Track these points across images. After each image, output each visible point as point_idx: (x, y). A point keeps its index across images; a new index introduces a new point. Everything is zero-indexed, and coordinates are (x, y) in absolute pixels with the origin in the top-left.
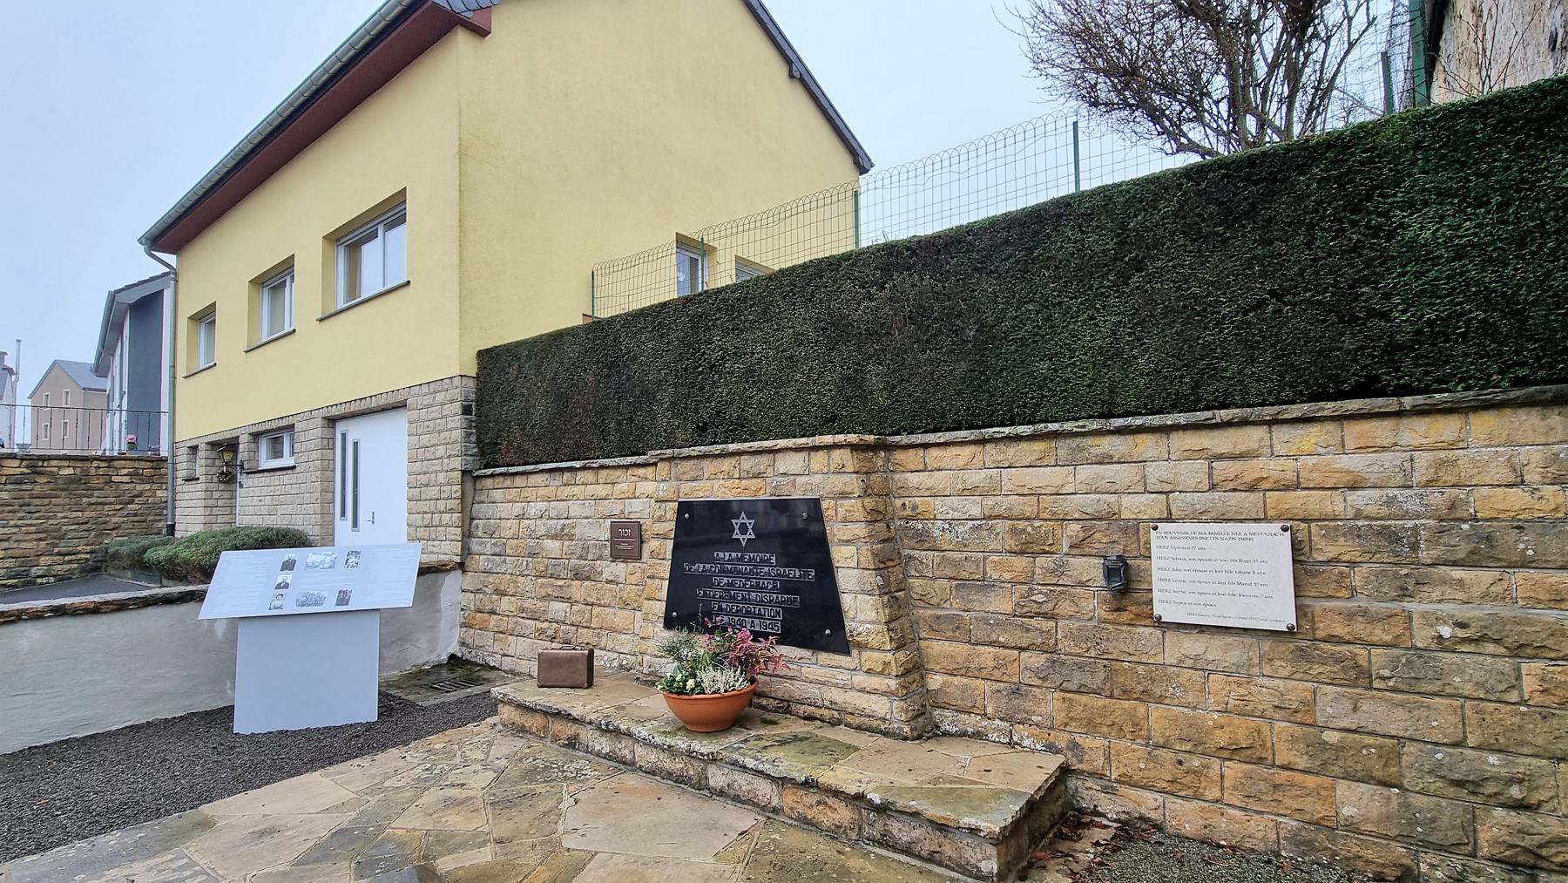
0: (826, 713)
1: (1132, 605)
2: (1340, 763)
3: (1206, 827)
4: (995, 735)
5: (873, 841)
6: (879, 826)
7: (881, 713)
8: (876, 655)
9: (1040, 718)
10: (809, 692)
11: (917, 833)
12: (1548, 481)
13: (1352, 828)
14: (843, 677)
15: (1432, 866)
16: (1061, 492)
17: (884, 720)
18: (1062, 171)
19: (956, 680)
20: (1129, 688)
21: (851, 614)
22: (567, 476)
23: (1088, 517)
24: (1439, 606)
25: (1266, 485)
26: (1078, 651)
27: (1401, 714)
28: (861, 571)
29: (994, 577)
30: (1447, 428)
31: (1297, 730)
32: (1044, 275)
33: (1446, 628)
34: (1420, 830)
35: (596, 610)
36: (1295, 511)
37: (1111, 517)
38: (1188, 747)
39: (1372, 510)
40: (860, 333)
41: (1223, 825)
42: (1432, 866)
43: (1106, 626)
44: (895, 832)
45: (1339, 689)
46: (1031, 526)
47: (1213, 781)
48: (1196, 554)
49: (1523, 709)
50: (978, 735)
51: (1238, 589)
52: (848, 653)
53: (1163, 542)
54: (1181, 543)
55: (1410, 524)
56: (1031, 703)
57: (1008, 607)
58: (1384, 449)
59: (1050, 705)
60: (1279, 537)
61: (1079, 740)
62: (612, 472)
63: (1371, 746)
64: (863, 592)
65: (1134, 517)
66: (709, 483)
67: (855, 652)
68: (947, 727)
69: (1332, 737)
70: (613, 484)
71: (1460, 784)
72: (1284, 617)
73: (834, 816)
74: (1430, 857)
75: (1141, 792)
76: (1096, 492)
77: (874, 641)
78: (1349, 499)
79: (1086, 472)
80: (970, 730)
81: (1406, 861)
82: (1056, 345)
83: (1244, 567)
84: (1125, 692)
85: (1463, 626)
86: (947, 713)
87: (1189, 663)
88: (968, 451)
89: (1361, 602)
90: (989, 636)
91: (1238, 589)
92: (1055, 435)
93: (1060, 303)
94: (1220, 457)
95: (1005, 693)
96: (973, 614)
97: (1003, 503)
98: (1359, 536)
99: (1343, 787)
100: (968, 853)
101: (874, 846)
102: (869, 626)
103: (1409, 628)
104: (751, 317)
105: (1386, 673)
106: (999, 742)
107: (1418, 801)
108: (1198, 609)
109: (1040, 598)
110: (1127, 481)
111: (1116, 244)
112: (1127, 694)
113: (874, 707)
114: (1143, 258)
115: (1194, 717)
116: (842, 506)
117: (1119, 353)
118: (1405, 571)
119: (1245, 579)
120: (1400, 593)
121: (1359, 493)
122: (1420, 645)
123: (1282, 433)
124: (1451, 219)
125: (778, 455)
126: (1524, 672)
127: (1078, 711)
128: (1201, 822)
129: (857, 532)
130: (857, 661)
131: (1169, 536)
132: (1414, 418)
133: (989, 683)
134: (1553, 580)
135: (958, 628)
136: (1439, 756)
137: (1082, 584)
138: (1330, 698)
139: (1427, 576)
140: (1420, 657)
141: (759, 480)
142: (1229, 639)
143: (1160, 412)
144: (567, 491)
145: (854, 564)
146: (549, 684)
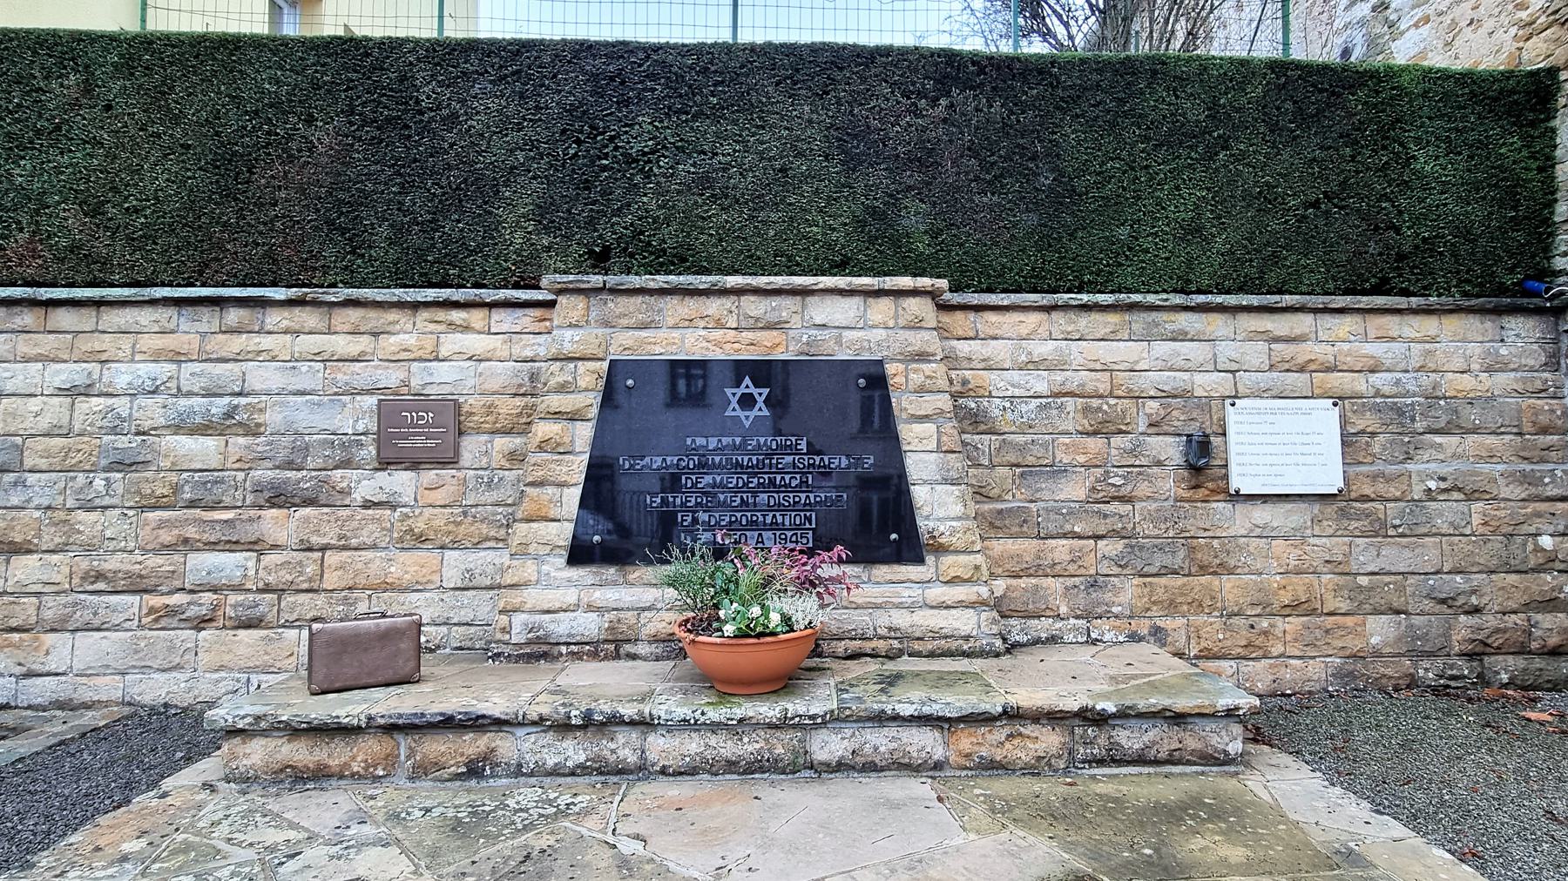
0: (881, 645)
1: (1208, 481)
2: (1371, 601)
3: (1274, 681)
4: (1071, 636)
5: (1090, 762)
6: (1102, 741)
7: (966, 629)
8: (963, 558)
9: (1120, 608)
10: (854, 621)
11: (1152, 735)
12: (1483, 369)
13: (1377, 654)
14: (914, 592)
15: (1426, 670)
16: (1137, 368)
17: (967, 638)
18: (426, 12)
19: (1023, 582)
20: (1206, 563)
21: (926, 511)
22: (234, 316)
23: (1164, 394)
24: (1427, 466)
25: (1313, 367)
26: (1157, 532)
27: (1407, 553)
28: (942, 455)
29: (1065, 461)
30: (1429, 325)
31: (1341, 580)
32: (1134, 132)
33: (1433, 482)
34: (1419, 643)
35: (332, 558)
36: (1335, 390)
37: (1184, 395)
38: (1258, 610)
39: (1386, 390)
40: (898, 156)
41: (1288, 676)
42: (1426, 670)
43: (1182, 504)
44: (1123, 742)
45: (1367, 540)
46: (1107, 404)
47: (1278, 638)
48: (1267, 428)
49: (1474, 538)
50: (1053, 640)
51: (1301, 459)
52: (920, 561)
53: (1240, 418)
54: (1256, 418)
55: (1409, 401)
56: (1110, 594)
57: (1081, 493)
58: (1393, 339)
59: (1128, 592)
60: (1330, 412)
61: (1159, 623)
62: (372, 314)
63: (1390, 583)
64: (947, 481)
65: (1206, 394)
66: (676, 334)
67: (930, 559)
68: (1017, 638)
69: (1363, 581)
70: (375, 334)
71: (1443, 601)
72: (1331, 480)
73: (1037, 746)
74: (1426, 664)
75: (1218, 663)
76: (1171, 370)
77: (956, 541)
78: (1370, 380)
79: (1163, 349)
80: (1044, 635)
81: (1412, 671)
82: (1140, 211)
83: (1305, 439)
84: (1201, 567)
85: (1443, 479)
86: (1013, 622)
87: (1258, 531)
88: (1033, 318)
89: (1379, 466)
90: (1061, 527)
91: (1301, 459)
92: (1132, 307)
93: (1147, 167)
94: (1277, 340)
95: (1082, 588)
96: (1041, 504)
97: (1075, 380)
98: (1380, 411)
99: (1372, 622)
100: (1215, 740)
101: (1090, 767)
102: (954, 524)
103: (1410, 485)
104: (715, 100)
105: (1397, 522)
106: (1077, 643)
107: (1417, 620)
108: (1271, 480)
109: (1118, 481)
110: (1201, 359)
111: (1206, 116)
112: (1204, 569)
113: (956, 624)
114: (1229, 137)
115: (1261, 582)
116: (915, 371)
117: (1199, 230)
118: (1407, 439)
119: (1306, 449)
120: (1406, 456)
121: (1377, 375)
122: (1416, 497)
123: (1328, 321)
124: (1442, 159)
125: (809, 299)
126: (1473, 511)
127: (1160, 594)
128: (1272, 677)
129: (940, 405)
130: (933, 570)
131: (1245, 411)
132: (1411, 316)
133: (1061, 580)
134: (1488, 441)
135: (1025, 521)
136: (1431, 582)
137: (1159, 464)
138: (1362, 548)
139: (1421, 442)
140: (1417, 506)
141: (775, 333)
142: (1289, 506)
143: (1228, 292)
144: (238, 343)
145: (933, 446)
146: (337, 685)
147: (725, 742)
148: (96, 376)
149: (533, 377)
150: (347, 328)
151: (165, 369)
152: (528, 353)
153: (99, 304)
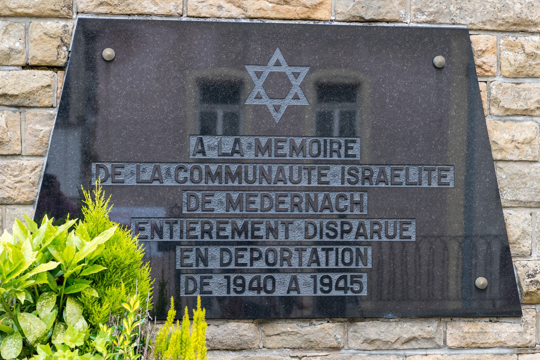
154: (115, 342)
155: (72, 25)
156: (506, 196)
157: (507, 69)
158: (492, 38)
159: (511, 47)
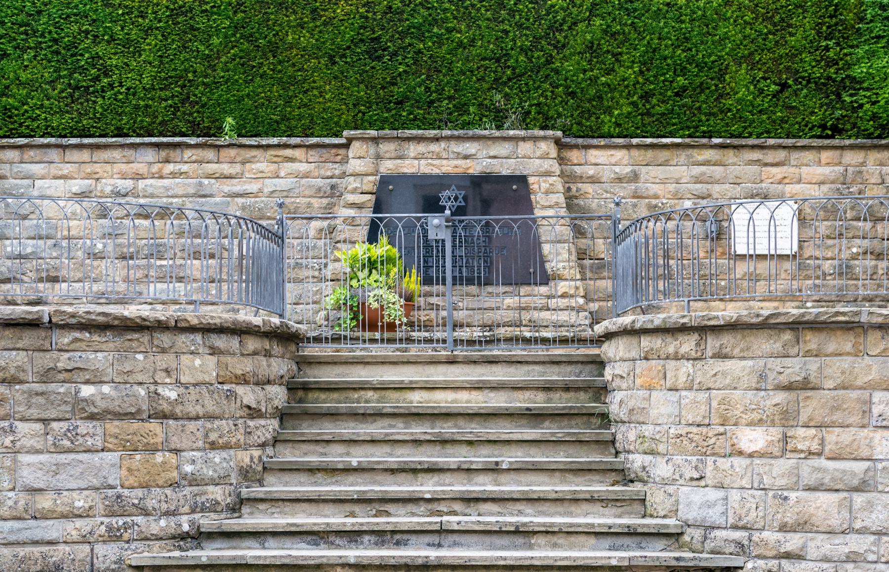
147: (599, 206)
148: (93, 187)
149: (333, 187)
150: (228, 160)
151: (129, 184)
152: (329, 173)
153: (98, 147)
154: (110, 492)
155: (378, 178)
156: (543, 238)
157: (543, 190)
158: (537, 178)
159: (545, 181)
